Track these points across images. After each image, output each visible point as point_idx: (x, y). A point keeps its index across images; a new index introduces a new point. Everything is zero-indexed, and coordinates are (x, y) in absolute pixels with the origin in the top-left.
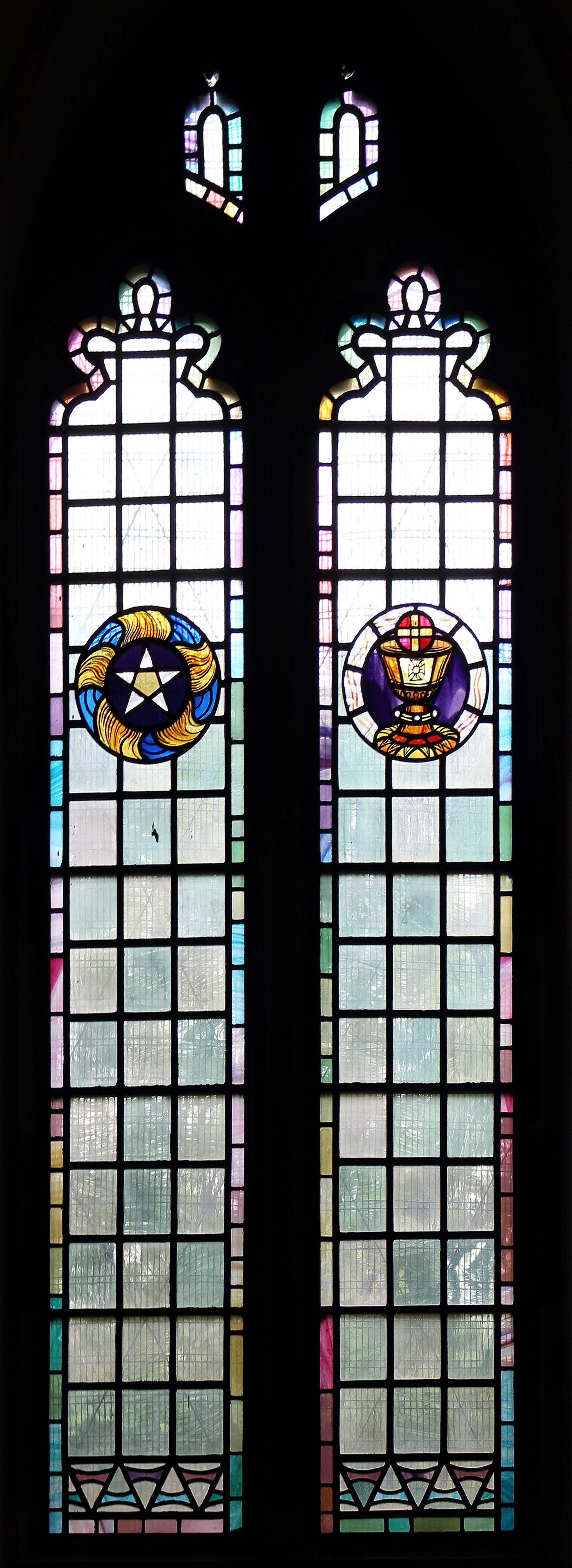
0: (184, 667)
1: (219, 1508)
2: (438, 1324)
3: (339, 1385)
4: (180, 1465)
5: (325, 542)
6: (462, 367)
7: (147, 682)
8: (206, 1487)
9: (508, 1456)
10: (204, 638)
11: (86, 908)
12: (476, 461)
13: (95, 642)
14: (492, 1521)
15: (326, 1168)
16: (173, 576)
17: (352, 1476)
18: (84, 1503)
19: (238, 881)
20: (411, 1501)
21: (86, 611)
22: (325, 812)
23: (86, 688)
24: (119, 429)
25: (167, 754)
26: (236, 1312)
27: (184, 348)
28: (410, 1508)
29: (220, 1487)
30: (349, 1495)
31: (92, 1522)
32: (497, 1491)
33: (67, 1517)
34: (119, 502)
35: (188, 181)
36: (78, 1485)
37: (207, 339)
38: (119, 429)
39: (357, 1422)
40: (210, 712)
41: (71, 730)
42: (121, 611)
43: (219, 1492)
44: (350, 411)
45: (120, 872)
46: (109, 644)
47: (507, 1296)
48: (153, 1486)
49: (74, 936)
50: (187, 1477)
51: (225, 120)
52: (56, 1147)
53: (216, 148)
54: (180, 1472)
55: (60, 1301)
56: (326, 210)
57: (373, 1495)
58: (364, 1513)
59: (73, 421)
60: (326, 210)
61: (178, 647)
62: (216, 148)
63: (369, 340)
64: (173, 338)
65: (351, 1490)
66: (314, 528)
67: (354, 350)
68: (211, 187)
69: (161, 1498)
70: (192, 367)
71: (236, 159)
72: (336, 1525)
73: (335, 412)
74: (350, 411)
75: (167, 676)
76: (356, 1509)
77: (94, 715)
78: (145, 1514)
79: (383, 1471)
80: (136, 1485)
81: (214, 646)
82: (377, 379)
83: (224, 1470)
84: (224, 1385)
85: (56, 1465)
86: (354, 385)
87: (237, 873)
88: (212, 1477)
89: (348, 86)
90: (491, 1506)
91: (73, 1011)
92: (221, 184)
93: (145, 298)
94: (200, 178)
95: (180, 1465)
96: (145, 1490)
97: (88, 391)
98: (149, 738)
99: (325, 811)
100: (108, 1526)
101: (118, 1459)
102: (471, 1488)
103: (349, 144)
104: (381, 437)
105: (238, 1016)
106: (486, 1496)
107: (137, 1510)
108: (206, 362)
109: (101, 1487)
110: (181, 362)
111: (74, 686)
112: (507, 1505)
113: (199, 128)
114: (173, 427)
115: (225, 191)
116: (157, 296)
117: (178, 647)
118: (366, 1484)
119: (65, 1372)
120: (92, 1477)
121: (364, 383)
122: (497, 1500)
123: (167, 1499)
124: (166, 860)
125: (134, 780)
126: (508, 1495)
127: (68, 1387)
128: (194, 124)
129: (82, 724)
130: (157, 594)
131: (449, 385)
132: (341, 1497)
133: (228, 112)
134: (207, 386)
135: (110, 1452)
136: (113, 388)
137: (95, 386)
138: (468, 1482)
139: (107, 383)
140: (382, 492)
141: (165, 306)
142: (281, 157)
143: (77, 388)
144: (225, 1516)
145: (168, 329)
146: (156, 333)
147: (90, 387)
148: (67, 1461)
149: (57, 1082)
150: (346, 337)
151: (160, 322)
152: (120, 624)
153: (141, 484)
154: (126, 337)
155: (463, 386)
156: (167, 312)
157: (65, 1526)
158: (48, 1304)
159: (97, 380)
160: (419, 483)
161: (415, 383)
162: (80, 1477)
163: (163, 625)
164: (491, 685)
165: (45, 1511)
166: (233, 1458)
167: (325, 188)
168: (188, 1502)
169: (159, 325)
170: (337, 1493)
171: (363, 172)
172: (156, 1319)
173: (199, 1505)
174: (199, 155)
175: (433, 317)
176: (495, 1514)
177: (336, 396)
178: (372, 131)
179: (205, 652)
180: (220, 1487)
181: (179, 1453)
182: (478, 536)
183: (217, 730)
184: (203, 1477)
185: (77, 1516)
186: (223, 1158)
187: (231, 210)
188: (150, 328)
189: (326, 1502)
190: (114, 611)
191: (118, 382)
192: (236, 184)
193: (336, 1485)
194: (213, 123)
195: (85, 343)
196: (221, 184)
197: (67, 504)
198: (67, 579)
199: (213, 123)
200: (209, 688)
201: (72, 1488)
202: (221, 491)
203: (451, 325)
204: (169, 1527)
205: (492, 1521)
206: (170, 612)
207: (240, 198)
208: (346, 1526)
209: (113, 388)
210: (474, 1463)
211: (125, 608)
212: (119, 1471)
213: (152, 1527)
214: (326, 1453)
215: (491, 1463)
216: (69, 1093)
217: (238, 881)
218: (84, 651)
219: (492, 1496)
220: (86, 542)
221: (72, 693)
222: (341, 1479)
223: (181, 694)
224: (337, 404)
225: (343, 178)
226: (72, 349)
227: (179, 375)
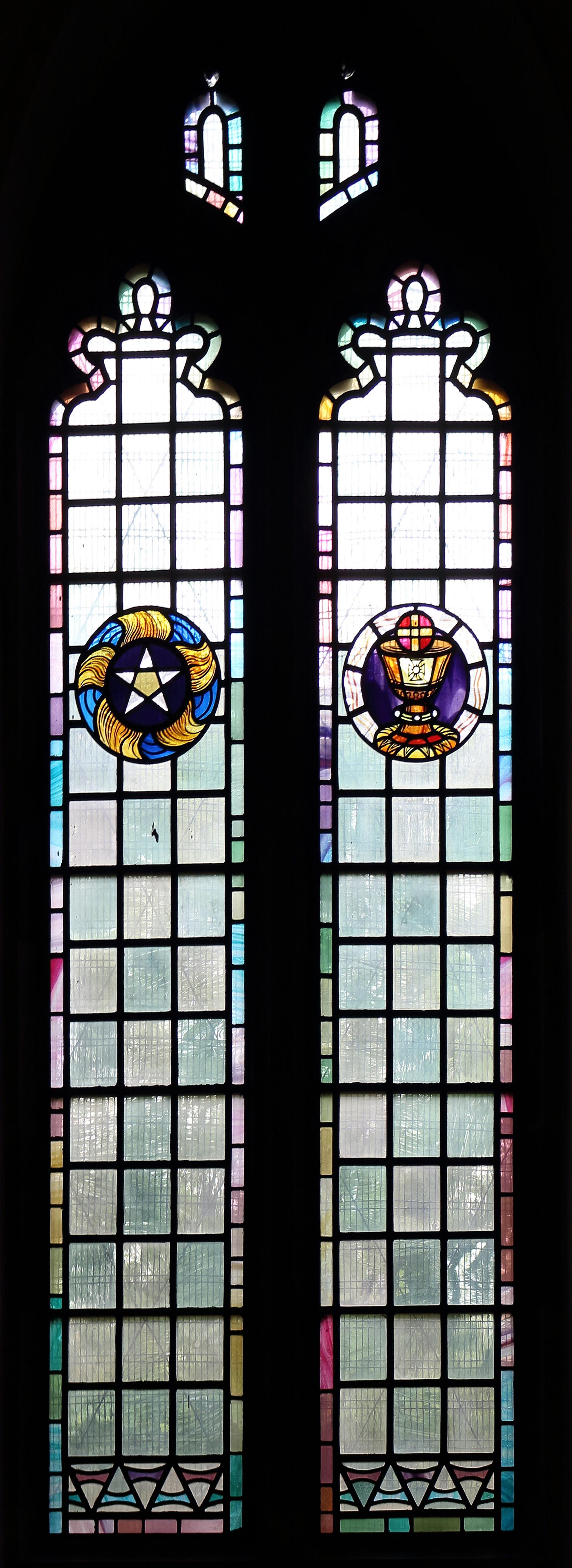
0: (184, 667)
1: (219, 1508)
2: (438, 1324)
3: (339, 1385)
4: (180, 1465)
5: (325, 542)
6: (462, 367)
7: (147, 682)
8: (206, 1487)
9: (508, 1456)
10: (204, 638)
11: (86, 908)
12: (476, 461)
13: (95, 642)
14: (492, 1521)
15: (326, 1168)
16: (173, 576)
17: (352, 1476)
18: (84, 1503)
19: (238, 881)
20: (411, 1501)
21: (86, 611)
22: (325, 812)
23: (86, 688)
24: (119, 429)
25: (167, 754)
26: (236, 1312)
27: (184, 348)
28: (410, 1508)
29: (220, 1487)
30: (349, 1495)
31: (92, 1522)
32: (497, 1491)
33: (67, 1517)
34: (119, 502)
35: (188, 181)
36: (78, 1485)
37: (207, 339)
38: (119, 429)
39: (357, 1422)
40: (210, 712)
41: (71, 730)
42: (121, 611)
43: (219, 1492)
44: (350, 411)
45: (120, 872)
46: (109, 644)
47: (507, 1296)
48: (153, 1486)
49: (74, 936)
50: (187, 1477)
51: (225, 120)
52: (56, 1147)
53: (216, 148)
54: (180, 1472)
55: (60, 1301)
56: (326, 210)
57: (373, 1495)
58: (364, 1513)
59: (73, 421)
60: (326, 210)
61: (178, 647)
62: (216, 148)
63: (369, 340)
64: (173, 338)
65: (351, 1490)
66: (314, 528)
67: (354, 350)
68: (211, 187)
69: (161, 1498)
70: (192, 367)
71: (236, 159)
72: (336, 1525)
73: (335, 412)
74: (350, 411)
75: (167, 676)
76: (356, 1509)
77: (94, 715)
78: (145, 1514)
79: (383, 1471)
80: (136, 1485)
81: (214, 646)
82: (377, 379)
83: (224, 1470)
84: (224, 1385)
86: (354, 385)
87: (237, 873)
88: (212, 1477)
89: (348, 86)
90: (491, 1506)
91: (73, 1011)
92: (221, 184)
93: (145, 298)
94: (200, 178)
95: (180, 1465)
96: (145, 1490)
97: (88, 391)
98: (149, 738)
100: (108, 1526)
101: (118, 1459)
102: (471, 1488)
103: (349, 144)
104: (381, 437)
105: (238, 1016)
106: (486, 1496)
107: (137, 1510)
108: (206, 362)
109: (101, 1487)
110: (181, 362)
111: (74, 686)
112: (507, 1505)
113: (199, 128)
114: (173, 427)
115: (225, 191)
116: (157, 296)
117: (178, 647)
118: (366, 1484)
119: (65, 1372)
120: (92, 1477)
121: (364, 383)
122: (497, 1500)
123: (167, 1499)
124: (166, 860)
125: (134, 780)
126: (508, 1495)
127: (68, 1387)
128: (194, 124)
129: (82, 724)
130: (157, 594)
131: (449, 385)
132: (341, 1497)
133: (228, 112)
134: (207, 386)
135: (110, 1452)
136: (113, 388)
137: (95, 386)
138: (468, 1482)
139: (107, 383)
140: (382, 492)
141: (165, 306)
142: (281, 157)
143: (77, 388)
144: (225, 1516)
145: (168, 329)
146: (156, 333)
147: (90, 387)
148: (67, 1461)
149: (57, 1082)
150: (346, 337)
151: (160, 322)
152: (120, 624)
153: (141, 484)
154: (126, 337)
155: (463, 386)
156: (167, 312)
157: (65, 1526)
159: (97, 380)
161: (415, 383)
162: (80, 1477)
163: (163, 625)
165: (45, 1511)
166: (233, 1458)
167: (325, 188)
168: (188, 1502)
169: (159, 325)
170: (337, 1493)
171: (363, 172)
172: (156, 1319)
173: (199, 1505)
174: (199, 155)
175: (433, 317)
176: (495, 1514)
177: (336, 396)
179: (205, 652)
180: (220, 1487)
181: (179, 1453)
182: (478, 536)
183: (217, 730)
184: (203, 1477)
185: (77, 1516)
186: (223, 1158)
187: (231, 210)
188: (150, 328)
189: (326, 1502)
190: (114, 611)
191: (118, 382)
192: (236, 184)
193: (336, 1485)
194: (213, 123)
195: (85, 343)
196: (221, 184)
197: (67, 504)
198: (67, 579)
199: (213, 123)
200: (209, 688)
201: (72, 1488)
202: (221, 491)
203: (451, 325)
204: (169, 1527)
205: (492, 1521)
206: (170, 612)
207: (240, 198)
208: (346, 1526)
209: (113, 388)
210: (474, 1463)
211: (125, 608)
212: (119, 1471)
213: (152, 1527)
214: (326, 1453)
215: (491, 1463)
216: (69, 1093)
217: (238, 881)
218: (84, 651)
219: (492, 1496)
220: (86, 542)
221: (72, 693)
222: (341, 1479)
223: (181, 694)
224: (337, 404)
225: (343, 178)
226: (72, 349)
227: (179, 375)
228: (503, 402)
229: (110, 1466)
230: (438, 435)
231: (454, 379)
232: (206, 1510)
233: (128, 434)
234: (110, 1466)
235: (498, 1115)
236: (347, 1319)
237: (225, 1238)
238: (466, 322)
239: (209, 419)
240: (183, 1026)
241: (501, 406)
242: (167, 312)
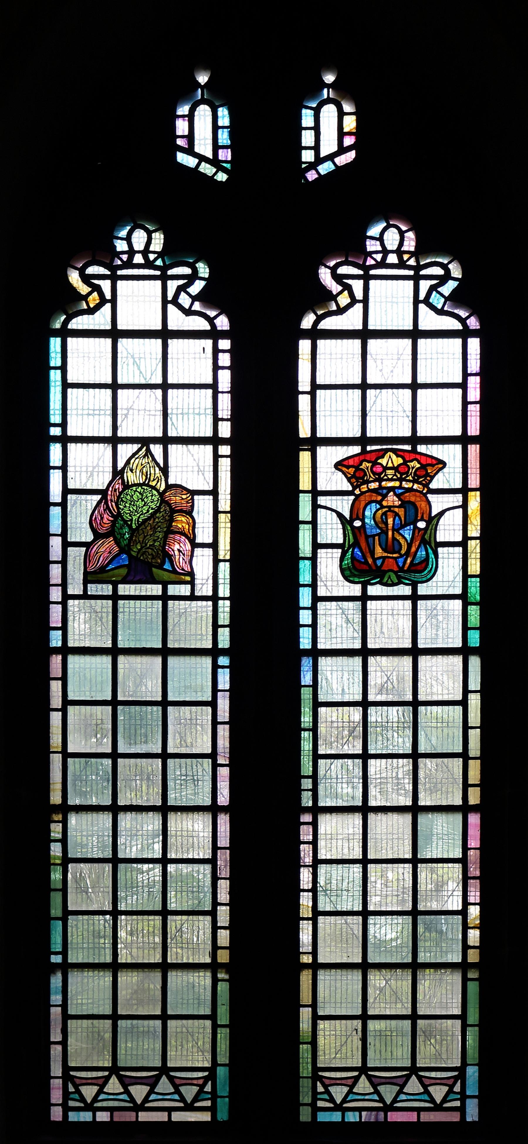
12: (444, 359)
17: (327, 1082)
26: (473, 965)
29: (457, 1088)
35: (153, 569)
36: (76, 1086)
38: (365, 335)
39: (335, 1046)
44: (78, 323)
49: (71, 697)
50: (427, 1082)
53: (203, 132)
62: (203, 132)
68: (202, 158)
70: (182, 293)
71: (224, 137)
72: (314, 1116)
73: (316, 323)
78: (388, 1108)
84: (213, 1017)
85: (56, 1070)
91: (70, 750)
92: (209, 155)
94: (190, 151)
97: (85, 307)
103: (327, 132)
106: (452, 1096)
113: (191, 117)
114: (165, 334)
115: (215, 162)
120: (89, 1082)
136: (108, 306)
140: (358, 381)
142: (265, 135)
143: (70, 302)
144: (462, 1110)
151: (152, 257)
153: (134, 377)
154: (121, 267)
158: (48, 431)
159: (344, 300)
160: (395, 363)
165: (48, 1105)
171: (342, 150)
174: (190, 137)
177: (320, 312)
178: (350, 123)
192: (225, 155)
196: (209, 155)
199: (329, 112)
201: (71, 1089)
203: (424, 262)
207: (304, 166)
209: (108, 306)
224: (319, 319)
228: (467, 314)
229: (356, 1074)
231: (175, 302)
232: (395, 1105)
233: (222, 339)
234: (356, 1074)
236: (124, 974)
238: (349, 259)
239: (351, 328)
240: (406, 764)
241: (468, 317)
242: (412, 249)
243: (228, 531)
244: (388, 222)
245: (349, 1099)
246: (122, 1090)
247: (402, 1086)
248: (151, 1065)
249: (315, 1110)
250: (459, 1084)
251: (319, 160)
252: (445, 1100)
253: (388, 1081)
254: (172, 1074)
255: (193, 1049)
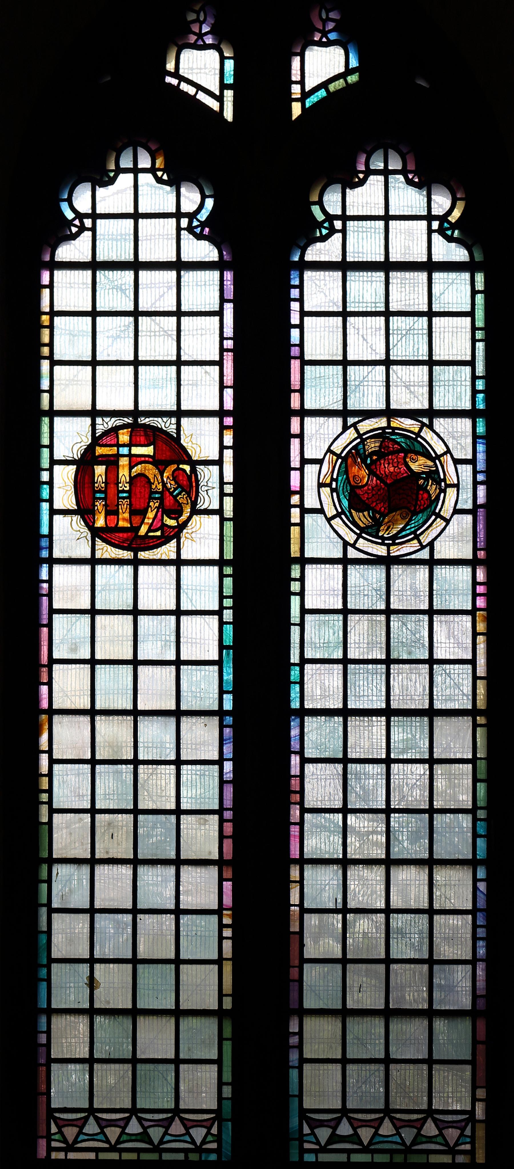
1: (468, 1147)
2: (426, 1023)
4: (139, 1115)
8: (204, 1131)
9: (480, 1112)
17: (61, 1123)
30: (355, 1137)
32: (473, 1137)
36: (312, 1128)
39: (320, 1089)
43: (213, 1135)
53: (322, 65)
56: (229, 114)
60: (229, 114)
62: (322, 65)
65: (60, 1132)
72: (301, 1157)
79: (381, 1120)
96: (113, 1133)
99: (295, 513)
101: (177, 1111)
103: (202, 69)
120: (366, 1124)
132: (53, 1137)
135: (128, 1105)
144: (472, 1153)
153: (130, 309)
164: (463, 488)
176: (218, 1151)
184: (368, 1124)
210: (200, 1115)
214: (294, 1104)
229: (127, 1115)
230: (340, 274)
235: (475, 880)
237: (304, 611)
243: (292, 455)
244: (177, 45)
245: (79, 1139)
246: (99, 1131)
247: (167, 1128)
248: (160, 1106)
249: (50, 1149)
250: (469, 1128)
251: (305, 95)
252: (204, 1142)
253: (368, 1124)
254: (351, 1115)
255: (202, 1089)
